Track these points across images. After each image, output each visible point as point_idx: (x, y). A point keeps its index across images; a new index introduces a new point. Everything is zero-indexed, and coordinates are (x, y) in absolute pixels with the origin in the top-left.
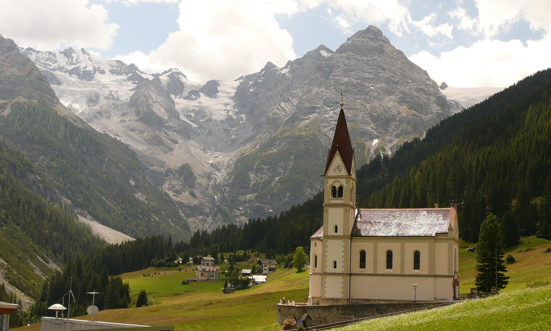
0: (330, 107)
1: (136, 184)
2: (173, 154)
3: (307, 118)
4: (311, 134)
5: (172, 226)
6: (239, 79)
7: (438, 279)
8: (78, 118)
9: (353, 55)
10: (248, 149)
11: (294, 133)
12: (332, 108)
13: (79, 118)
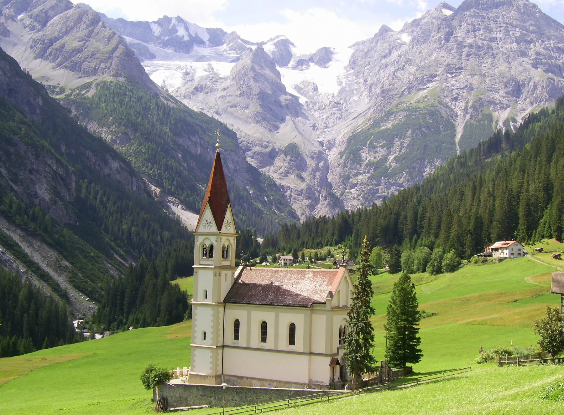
0: (451, 73)
1: (235, 167)
2: (278, 132)
3: (425, 87)
4: (430, 105)
5: (276, 214)
6: (354, 45)
7: (313, 357)
8: (171, 97)
9: (478, 13)
10: (360, 125)
11: (410, 105)
12: (454, 75)
13: (172, 96)
